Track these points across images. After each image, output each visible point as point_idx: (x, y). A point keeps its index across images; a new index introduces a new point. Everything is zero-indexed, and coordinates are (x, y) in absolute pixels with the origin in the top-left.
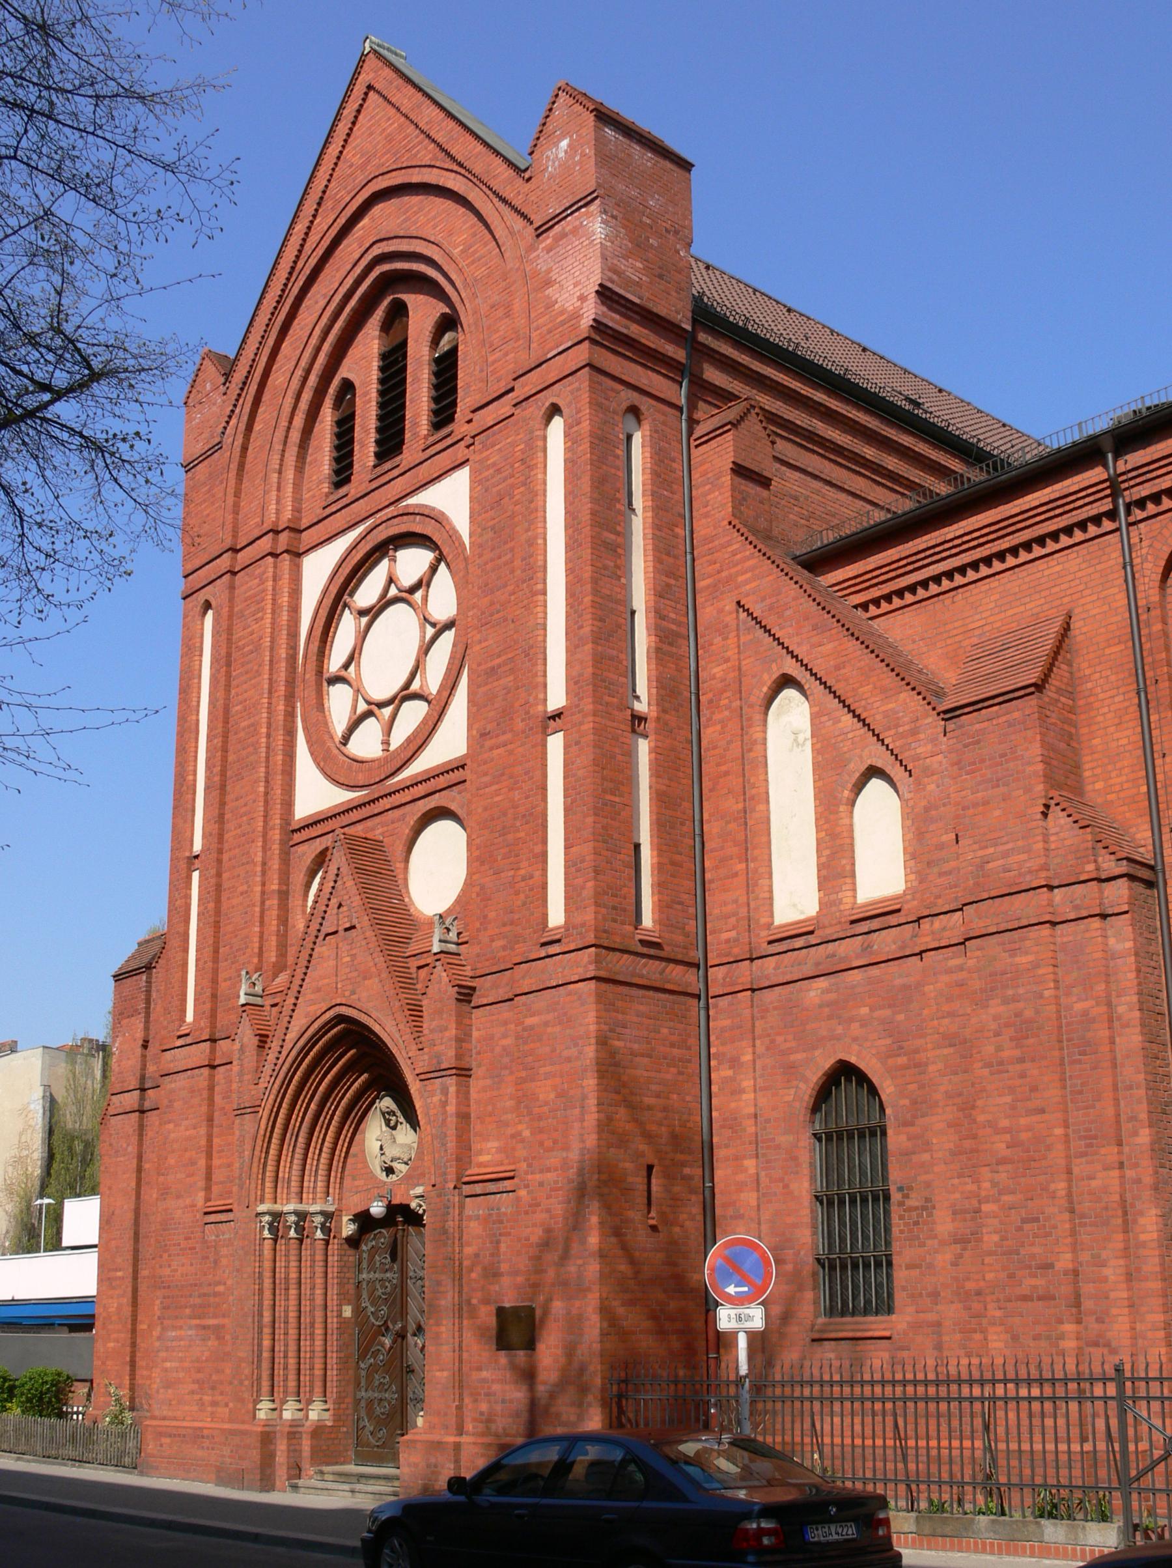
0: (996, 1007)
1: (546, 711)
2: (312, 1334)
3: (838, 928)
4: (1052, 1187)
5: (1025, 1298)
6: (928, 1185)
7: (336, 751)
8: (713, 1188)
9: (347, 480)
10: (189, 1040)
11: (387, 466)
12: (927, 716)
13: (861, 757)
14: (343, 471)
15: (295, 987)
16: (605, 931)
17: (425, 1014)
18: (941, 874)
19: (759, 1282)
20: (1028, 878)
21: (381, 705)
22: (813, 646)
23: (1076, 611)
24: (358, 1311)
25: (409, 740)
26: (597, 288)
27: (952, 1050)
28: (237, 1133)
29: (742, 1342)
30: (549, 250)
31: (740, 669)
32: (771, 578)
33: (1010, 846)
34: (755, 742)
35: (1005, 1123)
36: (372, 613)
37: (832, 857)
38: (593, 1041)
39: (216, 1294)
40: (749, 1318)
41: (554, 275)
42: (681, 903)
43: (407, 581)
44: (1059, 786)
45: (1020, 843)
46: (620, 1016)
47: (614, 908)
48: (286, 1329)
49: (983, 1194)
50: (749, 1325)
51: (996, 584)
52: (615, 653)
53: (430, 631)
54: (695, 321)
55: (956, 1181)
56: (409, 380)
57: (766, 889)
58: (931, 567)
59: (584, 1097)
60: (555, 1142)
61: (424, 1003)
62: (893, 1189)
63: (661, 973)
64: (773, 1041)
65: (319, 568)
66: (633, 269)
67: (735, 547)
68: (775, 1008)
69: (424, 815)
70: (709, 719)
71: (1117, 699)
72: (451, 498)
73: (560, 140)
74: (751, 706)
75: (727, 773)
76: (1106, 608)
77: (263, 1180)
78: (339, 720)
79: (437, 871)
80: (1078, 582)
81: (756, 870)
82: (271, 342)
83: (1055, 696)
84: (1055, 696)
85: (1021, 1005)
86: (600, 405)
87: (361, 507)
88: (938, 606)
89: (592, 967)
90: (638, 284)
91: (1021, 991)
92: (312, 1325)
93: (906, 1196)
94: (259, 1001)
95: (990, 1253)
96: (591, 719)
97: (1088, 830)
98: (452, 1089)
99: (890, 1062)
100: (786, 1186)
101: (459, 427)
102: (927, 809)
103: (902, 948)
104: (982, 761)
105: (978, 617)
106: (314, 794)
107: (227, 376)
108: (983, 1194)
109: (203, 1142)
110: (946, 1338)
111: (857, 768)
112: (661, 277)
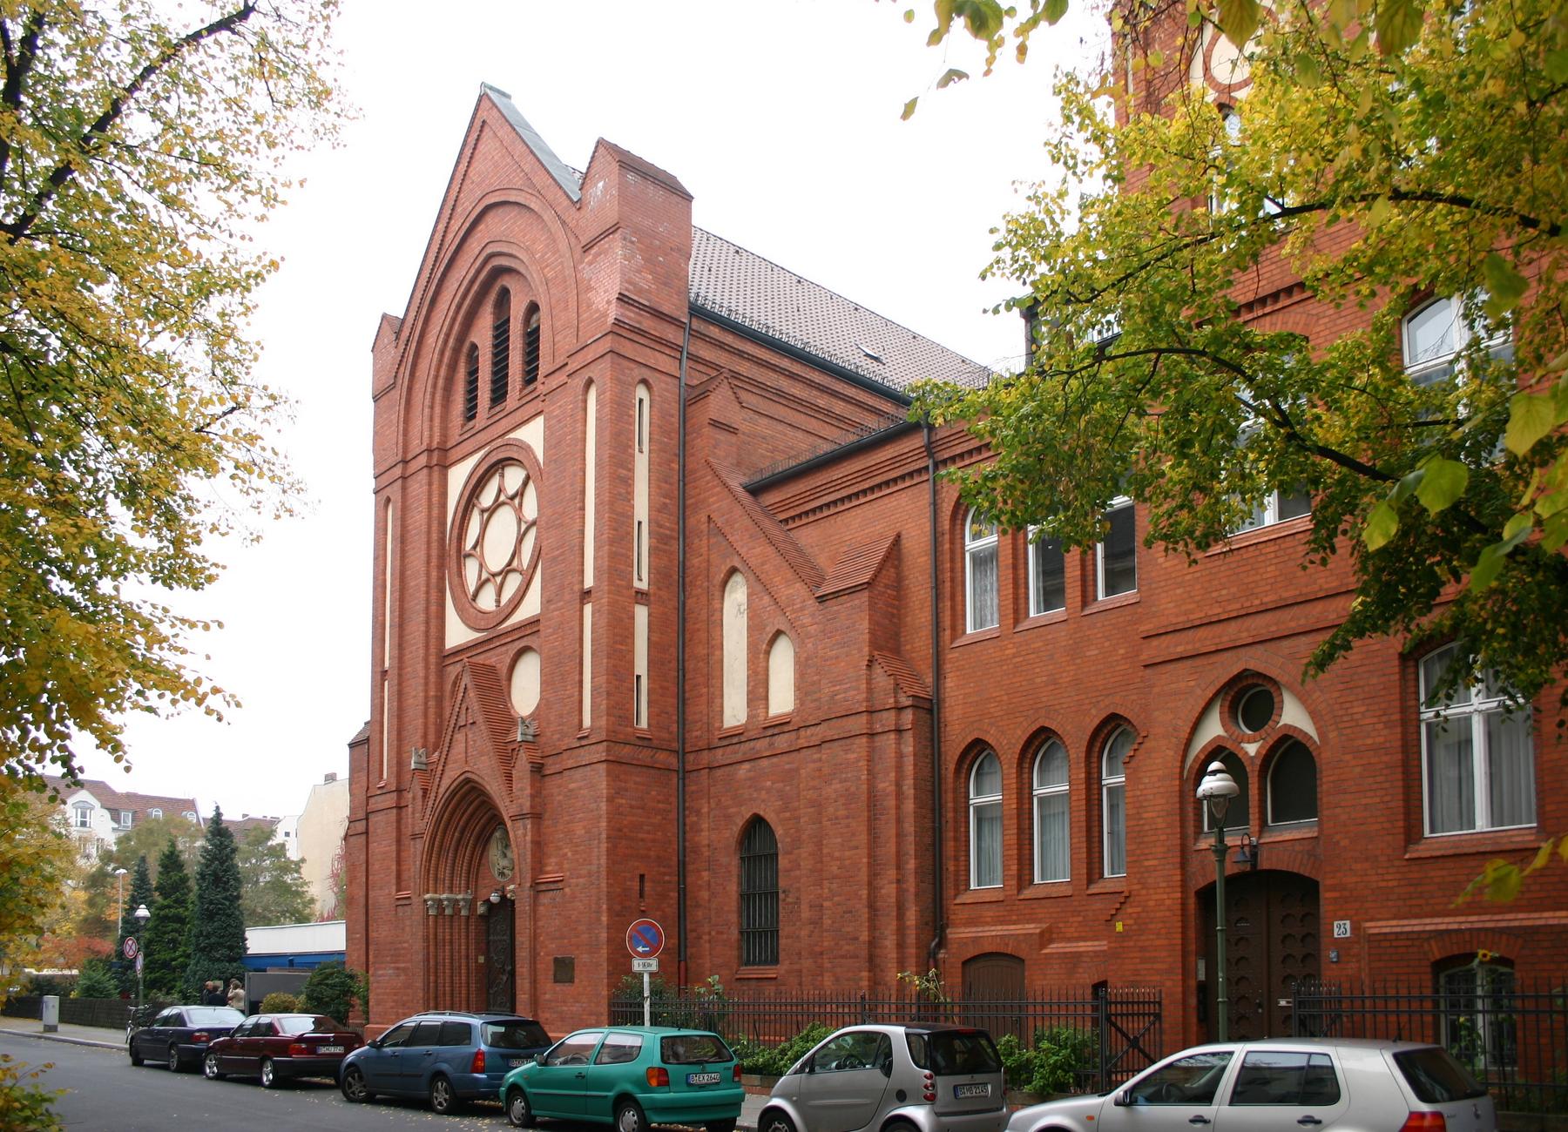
0: (836, 786)
5: (843, 957)
9: (473, 417)
11: (498, 409)
14: (471, 413)
21: (494, 575)
24: (488, 959)
25: (510, 601)
29: (646, 978)
30: (590, 264)
35: (837, 854)
36: (492, 511)
37: (755, 687)
43: (511, 490)
53: (524, 527)
66: (645, 281)
72: (533, 434)
78: (471, 585)
79: (526, 690)
82: (424, 312)
86: (619, 380)
87: (483, 437)
101: (541, 387)
102: (807, 659)
106: (457, 633)
111: (771, 630)
112: (665, 284)
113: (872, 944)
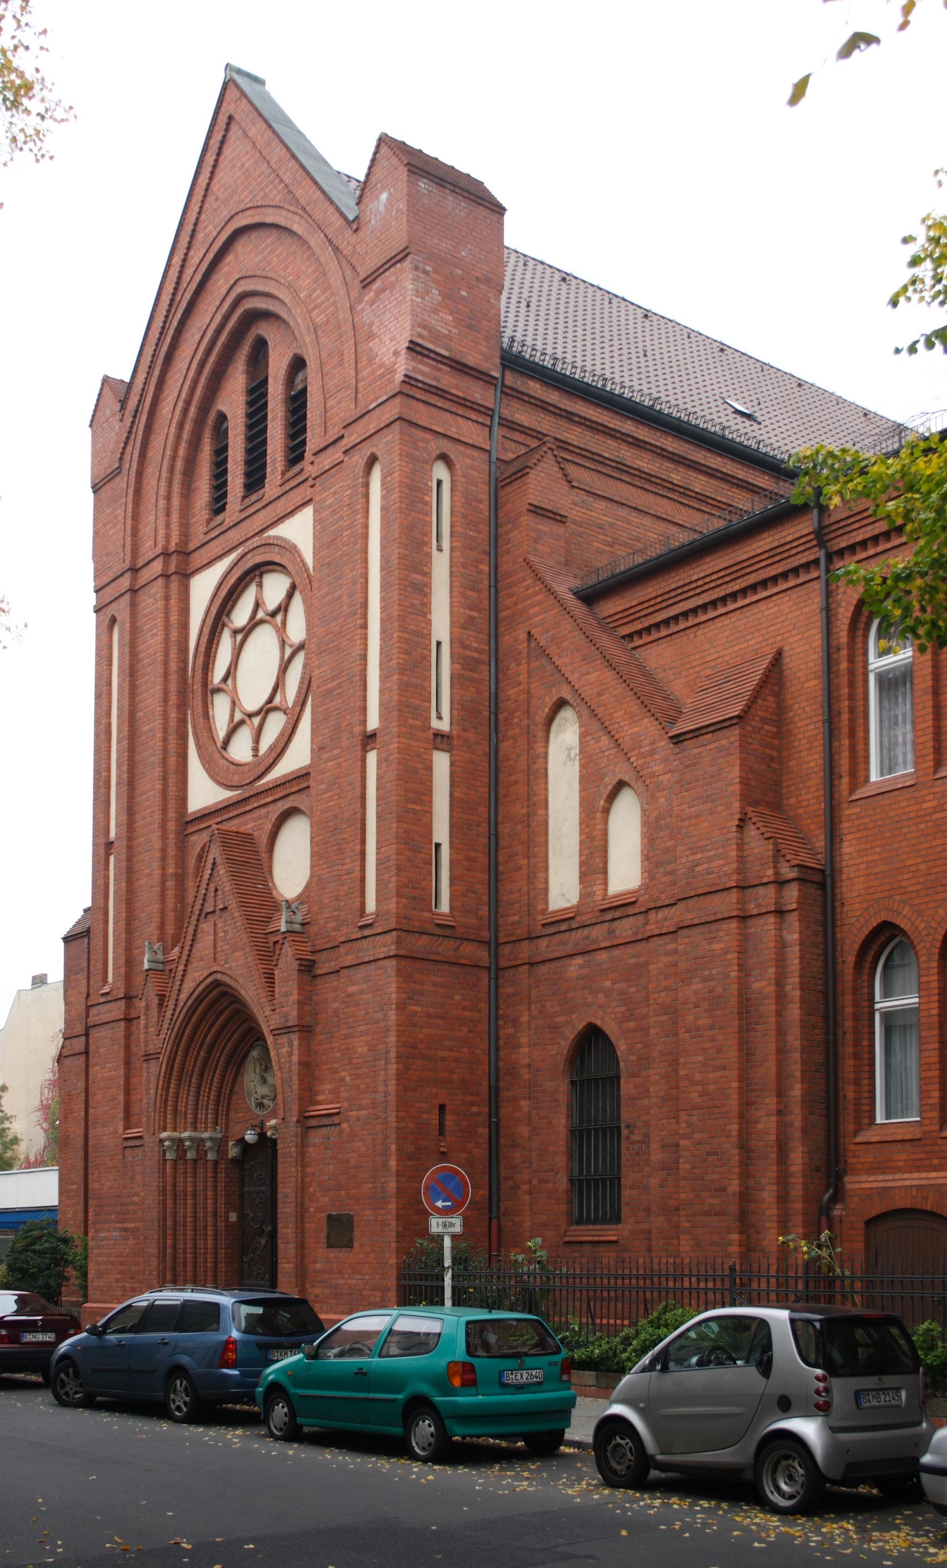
1: (365, 731)
2: (206, 1235)
3: (591, 915)
4: (728, 1127)
5: (706, 1214)
6: (647, 1124)
7: (217, 755)
8: (498, 1123)
9: (222, 509)
10: (109, 998)
11: (254, 498)
12: (662, 740)
13: (614, 772)
14: (218, 504)
15: (184, 957)
16: (406, 918)
17: (276, 981)
18: (665, 874)
19: (459, 1199)
20: (724, 879)
21: (250, 716)
22: (583, 675)
23: (786, 649)
24: (242, 1217)
26: (407, 344)
27: (666, 1017)
28: (145, 1075)
29: (447, 1242)
30: (372, 303)
31: (529, 692)
32: (553, 612)
33: (713, 852)
34: (538, 756)
35: (698, 1077)
36: (247, 631)
38: (394, 1006)
39: (133, 1203)
40: (452, 1225)
41: (375, 329)
42: (475, 892)
43: (271, 605)
44: (755, 803)
45: (720, 851)
46: (418, 987)
47: (414, 898)
48: (185, 1230)
49: (681, 1132)
50: (451, 1230)
51: (728, 621)
52: (419, 681)
54: (504, 367)
55: (665, 1121)
56: (270, 417)
57: (543, 880)
58: (681, 604)
59: (388, 1052)
60: (368, 1086)
61: (276, 972)
62: (623, 1126)
63: (455, 951)
64: (543, 1006)
65: (203, 587)
66: (444, 323)
67: (529, 582)
68: (546, 980)
69: (282, 813)
70: (505, 735)
71: (810, 727)
72: (299, 531)
73: (381, 193)
74: (536, 725)
75: (516, 782)
76: (807, 646)
77: (165, 1113)
78: (221, 726)
80: (788, 623)
81: (535, 866)
83: (759, 725)
84: (759, 725)
85: (714, 983)
86: (410, 456)
88: (685, 639)
89: (393, 947)
90: (448, 337)
91: (714, 972)
92: (205, 1227)
93: (631, 1132)
94: (160, 967)
95: (685, 1179)
96: (396, 740)
97: (771, 841)
98: (296, 1043)
99: (625, 1025)
100: (550, 1123)
101: (308, 468)
102: (658, 819)
103: (636, 933)
104: (697, 780)
105: (713, 650)
106: (203, 792)
107: (123, 403)
108: (681, 1132)
109: (122, 1081)
110: (654, 1243)
112: (470, 327)
113: (745, 1196)
